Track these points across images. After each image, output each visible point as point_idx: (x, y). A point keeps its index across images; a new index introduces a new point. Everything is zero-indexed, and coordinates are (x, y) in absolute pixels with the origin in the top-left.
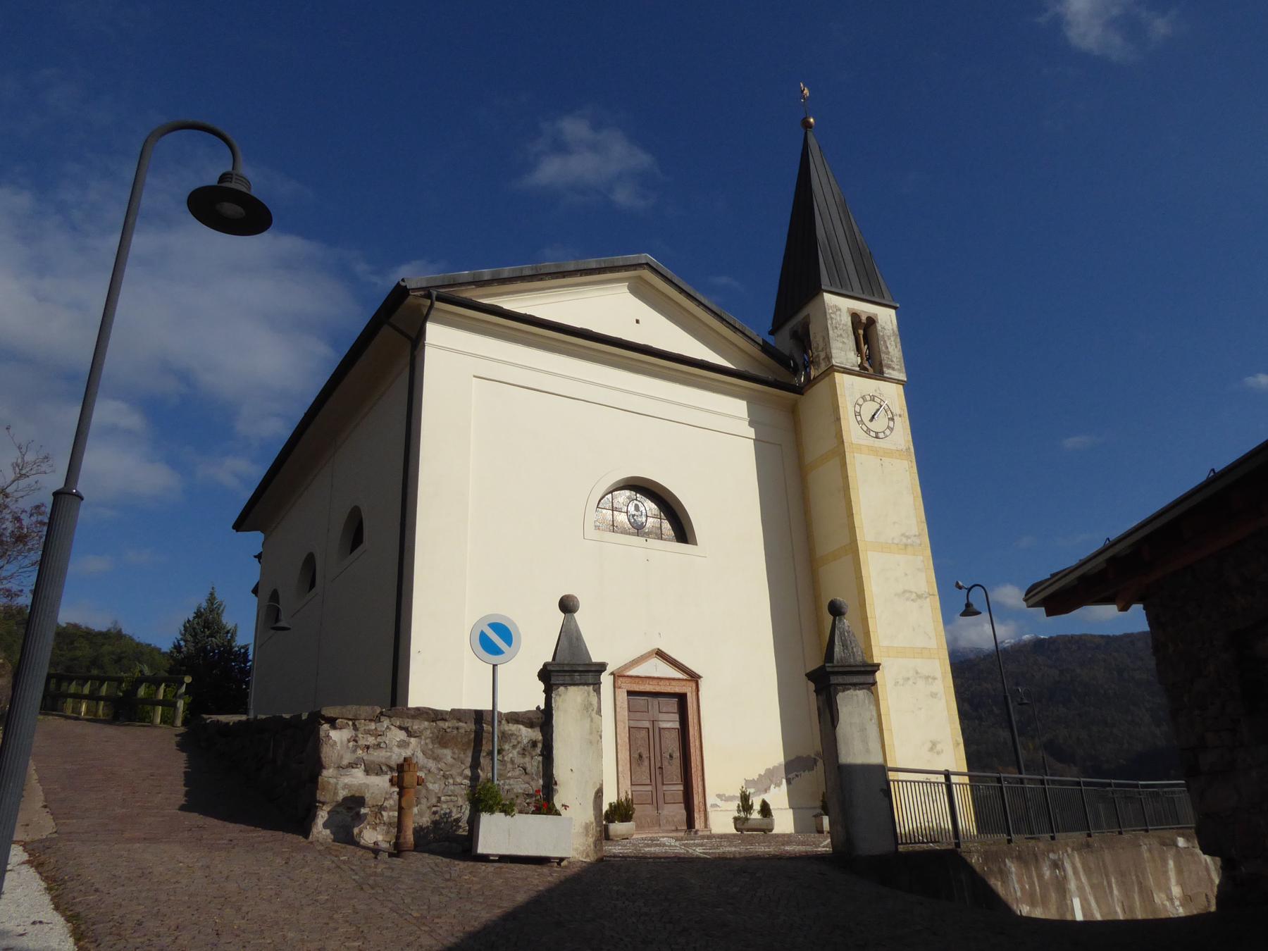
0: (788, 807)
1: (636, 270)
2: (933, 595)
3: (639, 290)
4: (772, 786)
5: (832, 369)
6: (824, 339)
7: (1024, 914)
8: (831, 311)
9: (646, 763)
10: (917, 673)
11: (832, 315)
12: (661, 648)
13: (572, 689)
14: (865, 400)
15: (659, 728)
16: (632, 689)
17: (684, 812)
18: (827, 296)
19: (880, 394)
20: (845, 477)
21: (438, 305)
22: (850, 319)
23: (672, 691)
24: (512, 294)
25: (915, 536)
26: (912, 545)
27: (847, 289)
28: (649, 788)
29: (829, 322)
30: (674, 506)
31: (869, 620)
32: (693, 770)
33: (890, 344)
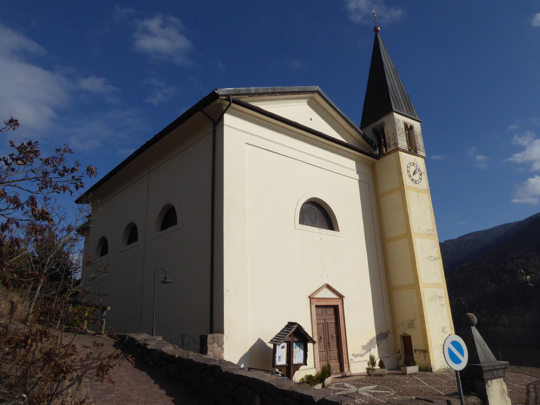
0: (378, 358)
1: (313, 94)
2: (440, 258)
3: (313, 104)
4: (372, 348)
5: (397, 149)
6: (393, 134)
8: (397, 122)
9: (323, 341)
10: (436, 295)
11: (397, 124)
12: (329, 284)
13: (494, 381)
14: (411, 165)
15: (327, 323)
16: (317, 304)
17: (338, 364)
18: (395, 114)
19: (416, 162)
20: (404, 202)
21: (233, 105)
22: (404, 125)
23: (333, 304)
24: (259, 101)
25: (432, 230)
26: (431, 235)
27: (402, 111)
28: (325, 353)
29: (396, 127)
30: (327, 211)
31: (417, 270)
32: (343, 343)
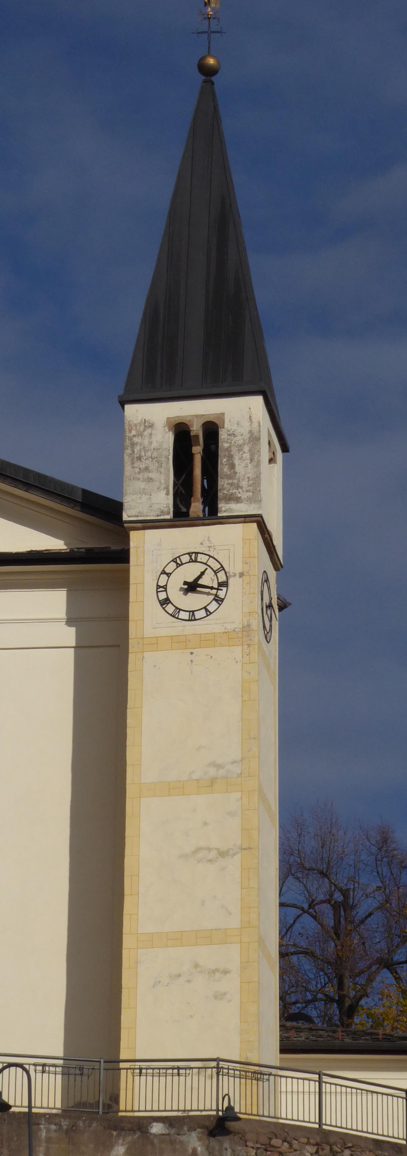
7: (124, 497)
33: (241, 458)
